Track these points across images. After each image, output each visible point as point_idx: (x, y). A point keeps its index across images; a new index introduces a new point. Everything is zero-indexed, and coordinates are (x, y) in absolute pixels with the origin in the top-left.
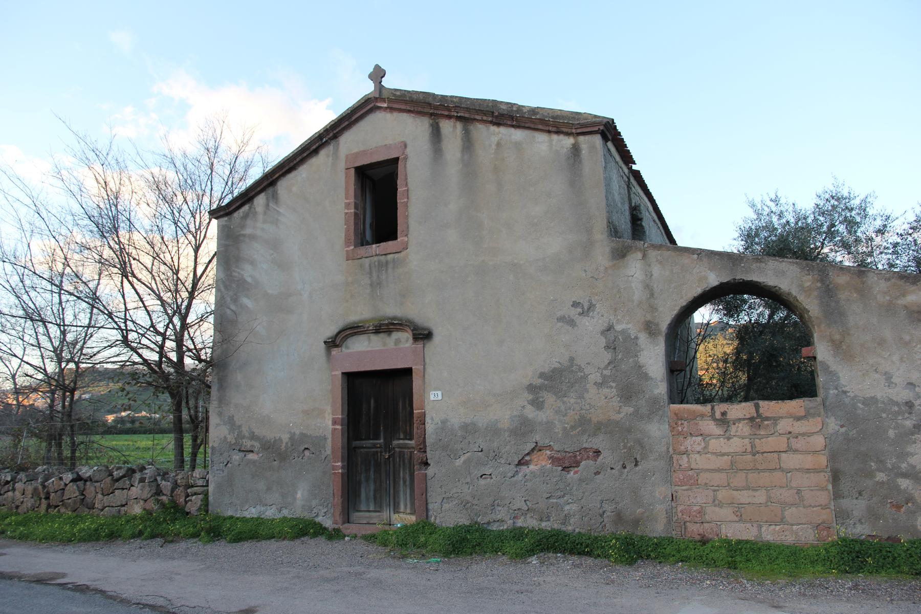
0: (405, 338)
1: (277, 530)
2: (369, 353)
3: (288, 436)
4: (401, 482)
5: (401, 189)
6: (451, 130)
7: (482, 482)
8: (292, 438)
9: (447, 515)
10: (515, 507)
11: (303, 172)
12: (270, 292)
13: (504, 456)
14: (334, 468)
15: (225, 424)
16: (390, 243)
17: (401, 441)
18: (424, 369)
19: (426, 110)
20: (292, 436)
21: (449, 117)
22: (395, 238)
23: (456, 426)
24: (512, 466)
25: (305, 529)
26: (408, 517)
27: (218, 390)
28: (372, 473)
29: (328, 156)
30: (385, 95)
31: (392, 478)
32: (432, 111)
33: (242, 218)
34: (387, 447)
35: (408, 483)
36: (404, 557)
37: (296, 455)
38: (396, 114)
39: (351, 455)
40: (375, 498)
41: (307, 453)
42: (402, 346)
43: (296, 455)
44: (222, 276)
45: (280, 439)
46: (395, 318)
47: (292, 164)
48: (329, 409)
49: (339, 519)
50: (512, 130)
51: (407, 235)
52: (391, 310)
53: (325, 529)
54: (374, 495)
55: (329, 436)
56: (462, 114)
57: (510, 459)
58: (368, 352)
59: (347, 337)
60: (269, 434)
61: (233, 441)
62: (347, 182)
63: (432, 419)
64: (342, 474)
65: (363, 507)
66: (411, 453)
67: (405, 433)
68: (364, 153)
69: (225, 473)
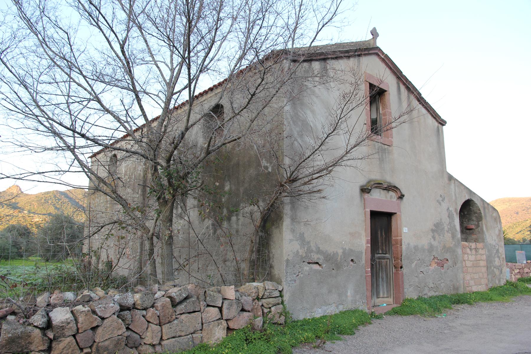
2: (381, 201)
4: (381, 280)
8: (344, 253)
15: (297, 240)
17: (379, 255)
20: (344, 250)
27: (291, 210)
35: (385, 279)
48: (363, 233)
55: (364, 251)
60: (330, 249)
66: (387, 262)
67: (382, 250)
69: (297, 282)
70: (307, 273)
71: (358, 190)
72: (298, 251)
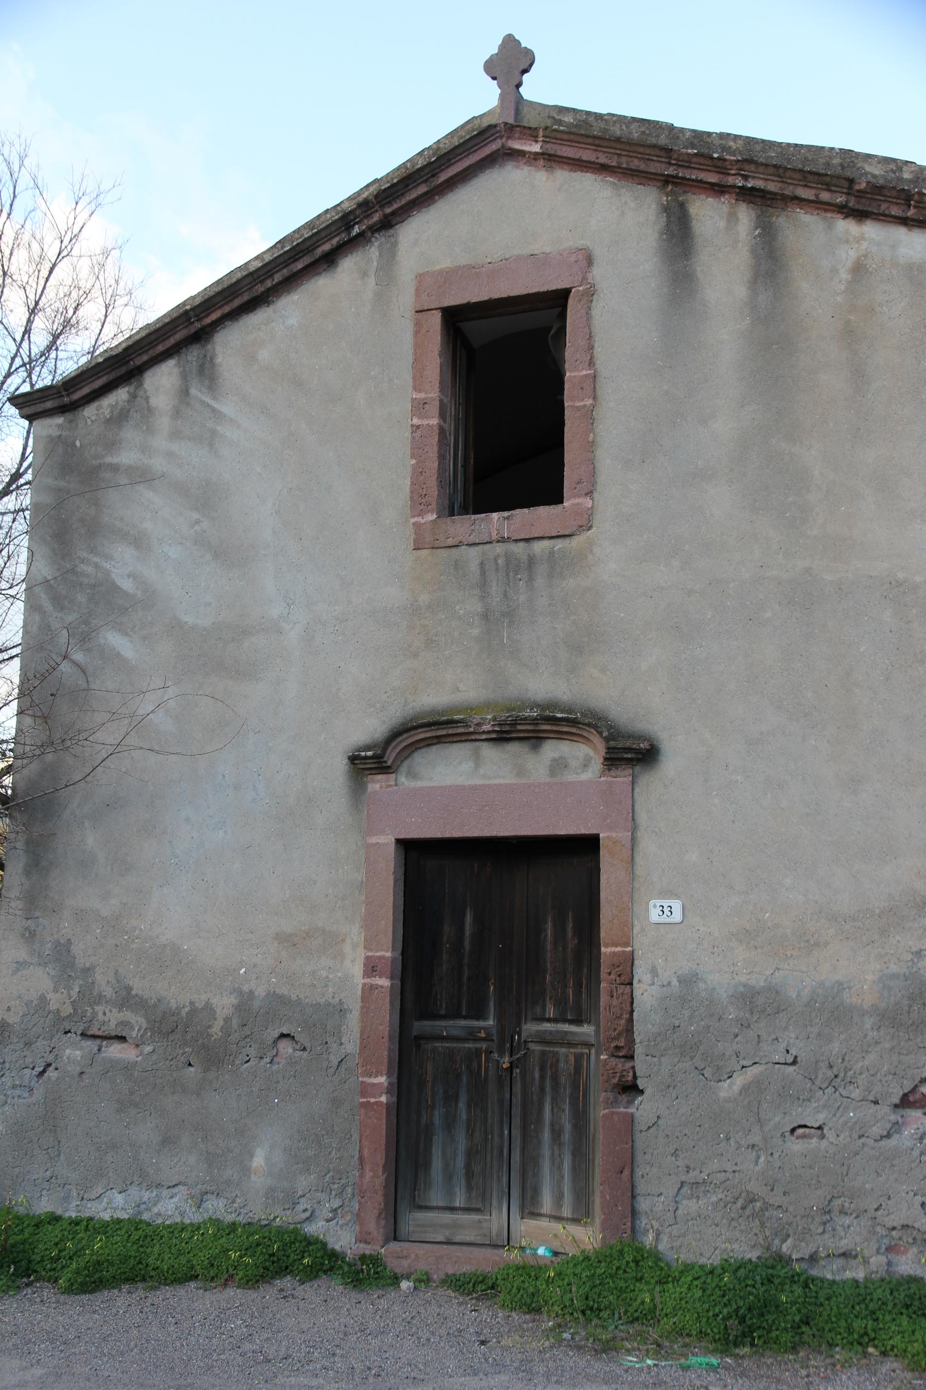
0: (581, 759)
1: (203, 1256)
2: (475, 792)
3: (233, 1000)
4: (546, 1136)
5: (573, 374)
6: (722, 224)
7: (796, 1146)
9: (694, 1230)
10: (895, 1220)
11: (290, 312)
12: (189, 619)
13: (862, 1080)
14: (365, 1090)
16: (543, 511)
17: (547, 1026)
18: (633, 839)
19: (654, 167)
21: (719, 190)
22: (555, 496)
23: (723, 994)
24: (884, 1110)
25: (282, 1257)
26: (576, 1230)
27: (27, 872)
28: (462, 1105)
29: (364, 274)
30: (531, 119)
31: (517, 1121)
32: (671, 171)
33: (108, 421)
34: (507, 1038)
35: (567, 1137)
36: (607, 1348)
37: (253, 1052)
38: (562, 175)
39: (408, 1054)
40: (469, 1174)
41: (286, 1047)
42: (570, 777)
43: (253, 1052)
44: (44, 570)
45: (208, 1008)
46: (553, 705)
47: (260, 289)
48: (355, 933)
50: (900, 233)
51: (589, 494)
52: (541, 684)
53: (334, 1255)
54: (468, 1166)
55: (355, 1006)
56: (759, 184)
57: (877, 1088)
58: (474, 788)
60: (177, 995)
61: (68, 1010)
62: (418, 346)
63: (654, 971)
64: (388, 1105)
65: (436, 1198)
67: (561, 1003)
68: (469, 272)
69: (39, 1094)
70: (75, 1070)
71: (341, 765)
72: (43, 999)
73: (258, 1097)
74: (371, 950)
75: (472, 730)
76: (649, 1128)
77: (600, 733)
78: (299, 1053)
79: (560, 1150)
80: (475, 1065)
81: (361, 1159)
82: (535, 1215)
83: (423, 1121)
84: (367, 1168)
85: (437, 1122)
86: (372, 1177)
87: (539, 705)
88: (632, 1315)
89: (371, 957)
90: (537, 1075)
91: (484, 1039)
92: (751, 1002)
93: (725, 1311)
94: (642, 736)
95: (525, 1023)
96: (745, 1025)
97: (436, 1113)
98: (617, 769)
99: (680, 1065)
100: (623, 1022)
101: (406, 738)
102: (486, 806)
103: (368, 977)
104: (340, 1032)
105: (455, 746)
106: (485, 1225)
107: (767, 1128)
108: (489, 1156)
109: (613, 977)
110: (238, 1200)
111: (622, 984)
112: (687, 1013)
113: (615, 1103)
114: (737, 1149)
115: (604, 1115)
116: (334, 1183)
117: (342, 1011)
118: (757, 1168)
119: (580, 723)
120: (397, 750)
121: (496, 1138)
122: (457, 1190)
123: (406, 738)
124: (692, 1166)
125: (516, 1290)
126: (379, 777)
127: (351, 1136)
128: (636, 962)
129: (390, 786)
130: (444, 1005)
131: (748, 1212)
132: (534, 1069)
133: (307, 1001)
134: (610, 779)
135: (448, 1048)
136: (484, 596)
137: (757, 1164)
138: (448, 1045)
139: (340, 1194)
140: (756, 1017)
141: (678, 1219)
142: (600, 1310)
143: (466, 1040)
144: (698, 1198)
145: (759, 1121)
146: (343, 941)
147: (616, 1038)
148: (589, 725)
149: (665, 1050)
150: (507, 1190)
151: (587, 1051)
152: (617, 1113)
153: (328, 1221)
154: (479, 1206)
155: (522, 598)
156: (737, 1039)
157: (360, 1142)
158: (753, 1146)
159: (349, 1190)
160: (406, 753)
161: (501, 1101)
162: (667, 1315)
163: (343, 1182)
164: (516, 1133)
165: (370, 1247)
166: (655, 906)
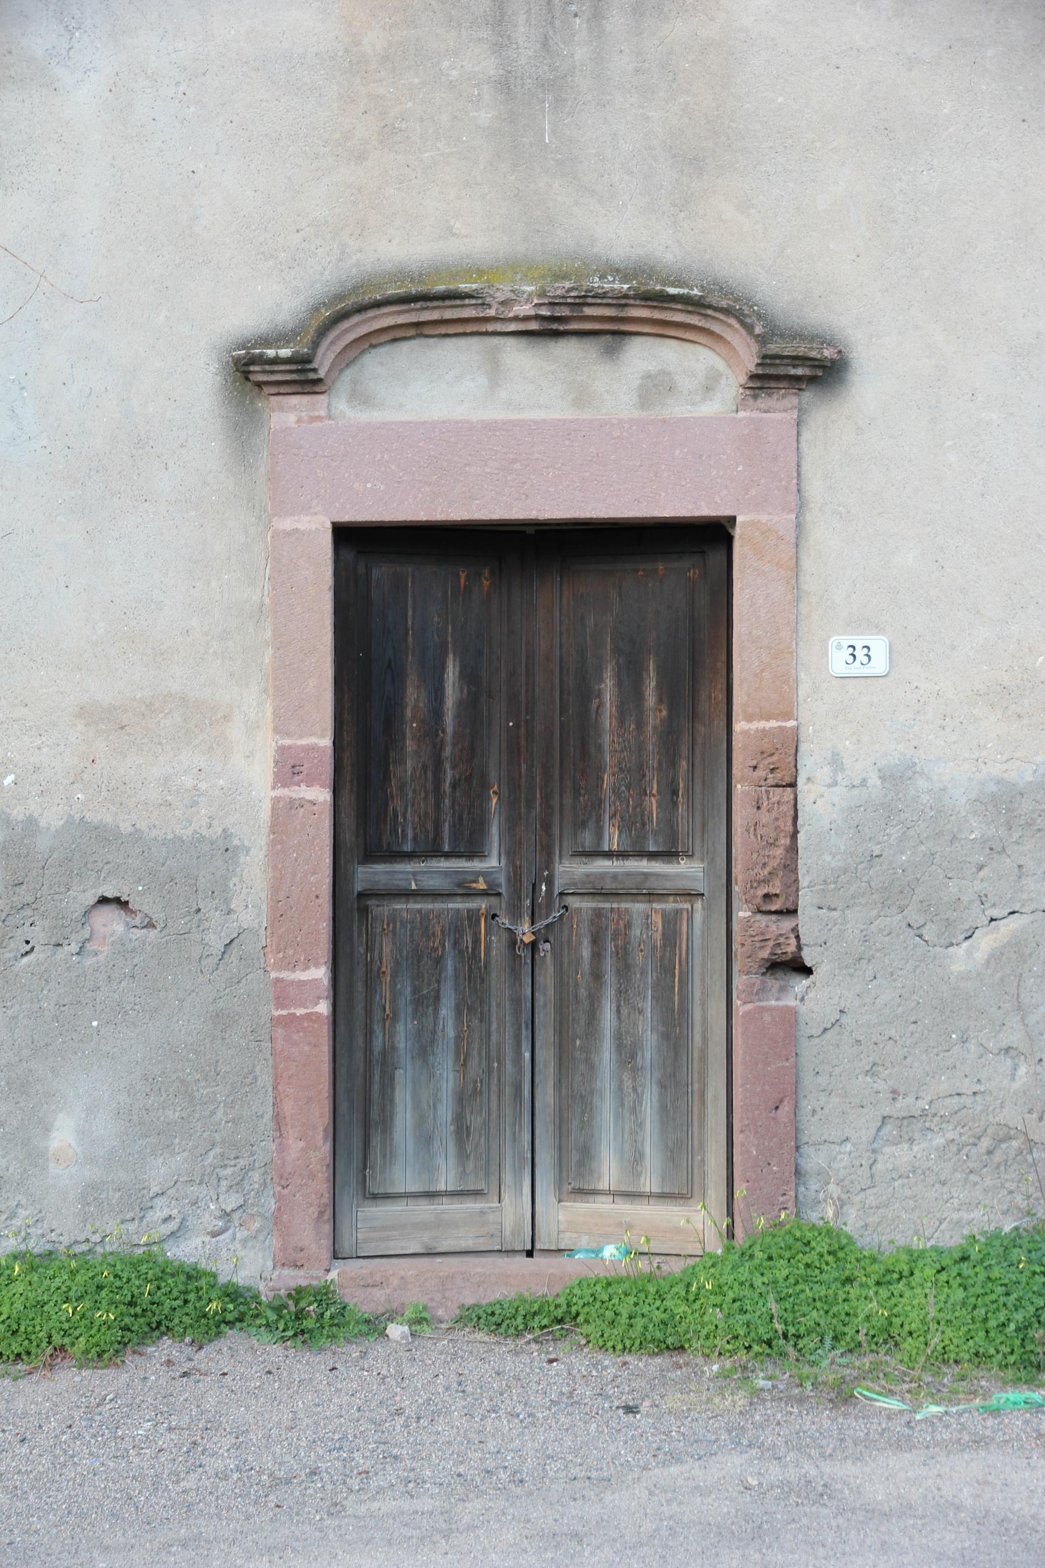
2: (486, 434)
14: (282, 993)
18: (799, 526)
25: (153, 1308)
28: (446, 1011)
31: (546, 1035)
34: (529, 889)
37: (38, 935)
40: (462, 1131)
41: (111, 922)
42: (678, 410)
43: (38, 935)
49: (313, 1239)
52: (623, 230)
58: (491, 427)
59: (369, 341)
63: (836, 762)
65: (403, 1176)
66: (671, 921)
67: (634, 823)
71: (203, 379)
73: (56, 1018)
74: (289, 735)
75: (492, 312)
76: (825, 1030)
77: (749, 328)
78: (139, 933)
79: (634, 1080)
80: (468, 940)
81: (278, 1120)
82: (582, 1193)
83: (378, 1044)
84: (291, 1135)
85: (402, 1045)
86: (303, 1150)
87: (617, 270)
88: (853, 1339)
89: (290, 747)
90: (586, 952)
91: (484, 894)
92: (1008, 810)
93: (1019, 1316)
94: (817, 336)
95: (560, 863)
96: (996, 849)
97: (400, 1028)
98: (770, 395)
99: (882, 922)
100: (779, 852)
101: (357, 324)
102: (514, 461)
103: (285, 785)
104: (225, 889)
105: (449, 343)
106: (491, 1217)
107: (1032, 1020)
108: (494, 1098)
109: (761, 773)
110: (22, 1213)
111: (777, 786)
112: (895, 832)
113: (762, 992)
114: (980, 1057)
115: (747, 1014)
116: (225, 1166)
117: (228, 850)
118: (1016, 1085)
119: (710, 307)
120: (338, 348)
121: (509, 1067)
122: (441, 1161)
123: (357, 324)
124: (902, 1090)
125: (639, 1321)
126: (295, 400)
127: (255, 1078)
128: (803, 747)
129: (319, 418)
130: (410, 835)
131: (998, 1157)
132: (580, 944)
133: (154, 833)
134: (756, 415)
135: (419, 911)
136: (499, 47)
137: (1013, 1079)
138: (418, 906)
139: (237, 1185)
140: (1015, 836)
141: (877, 1178)
142: (798, 1337)
143: (451, 895)
144: (911, 1141)
145: (1019, 1008)
146: (227, 718)
147: (765, 881)
148: (727, 311)
149: (853, 897)
150: (529, 1156)
151: (687, 906)
152: (770, 1009)
153: (214, 1234)
154: (481, 1185)
155: (581, 53)
156: (981, 874)
157: (275, 1088)
158: (1008, 1050)
159: (256, 1176)
160: (351, 355)
161: (517, 1002)
162: (911, 1333)
163: (242, 1162)
164: (546, 1056)
165: (301, 1273)
166: (839, 647)
